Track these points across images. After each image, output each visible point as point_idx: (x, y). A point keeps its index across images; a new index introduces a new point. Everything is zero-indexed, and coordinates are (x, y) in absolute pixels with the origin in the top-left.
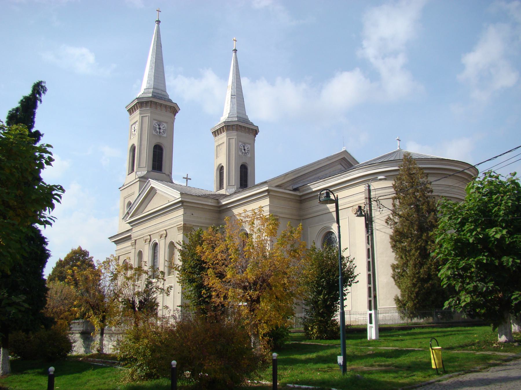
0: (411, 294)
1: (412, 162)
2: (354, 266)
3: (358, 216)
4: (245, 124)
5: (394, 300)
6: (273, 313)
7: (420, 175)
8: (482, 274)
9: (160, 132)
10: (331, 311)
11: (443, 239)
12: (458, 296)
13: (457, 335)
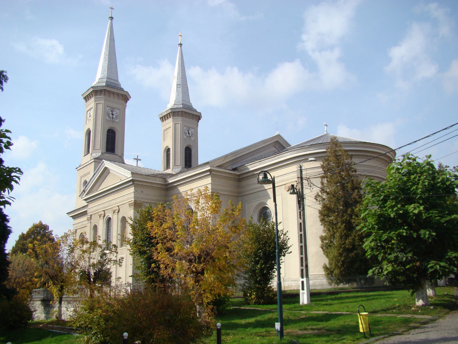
0: (338, 262)
1: (338, 145)
2: (287, 238)
3: (291, 193)
4: (189, 110)
5: (322, 268)
6: (217, 284)
7: (346, 157)
8: (402, 246)
9: (113, 118)
10: (267, 278)
11: (368, 214)
12: (381, 266)
13: (379, 299)
